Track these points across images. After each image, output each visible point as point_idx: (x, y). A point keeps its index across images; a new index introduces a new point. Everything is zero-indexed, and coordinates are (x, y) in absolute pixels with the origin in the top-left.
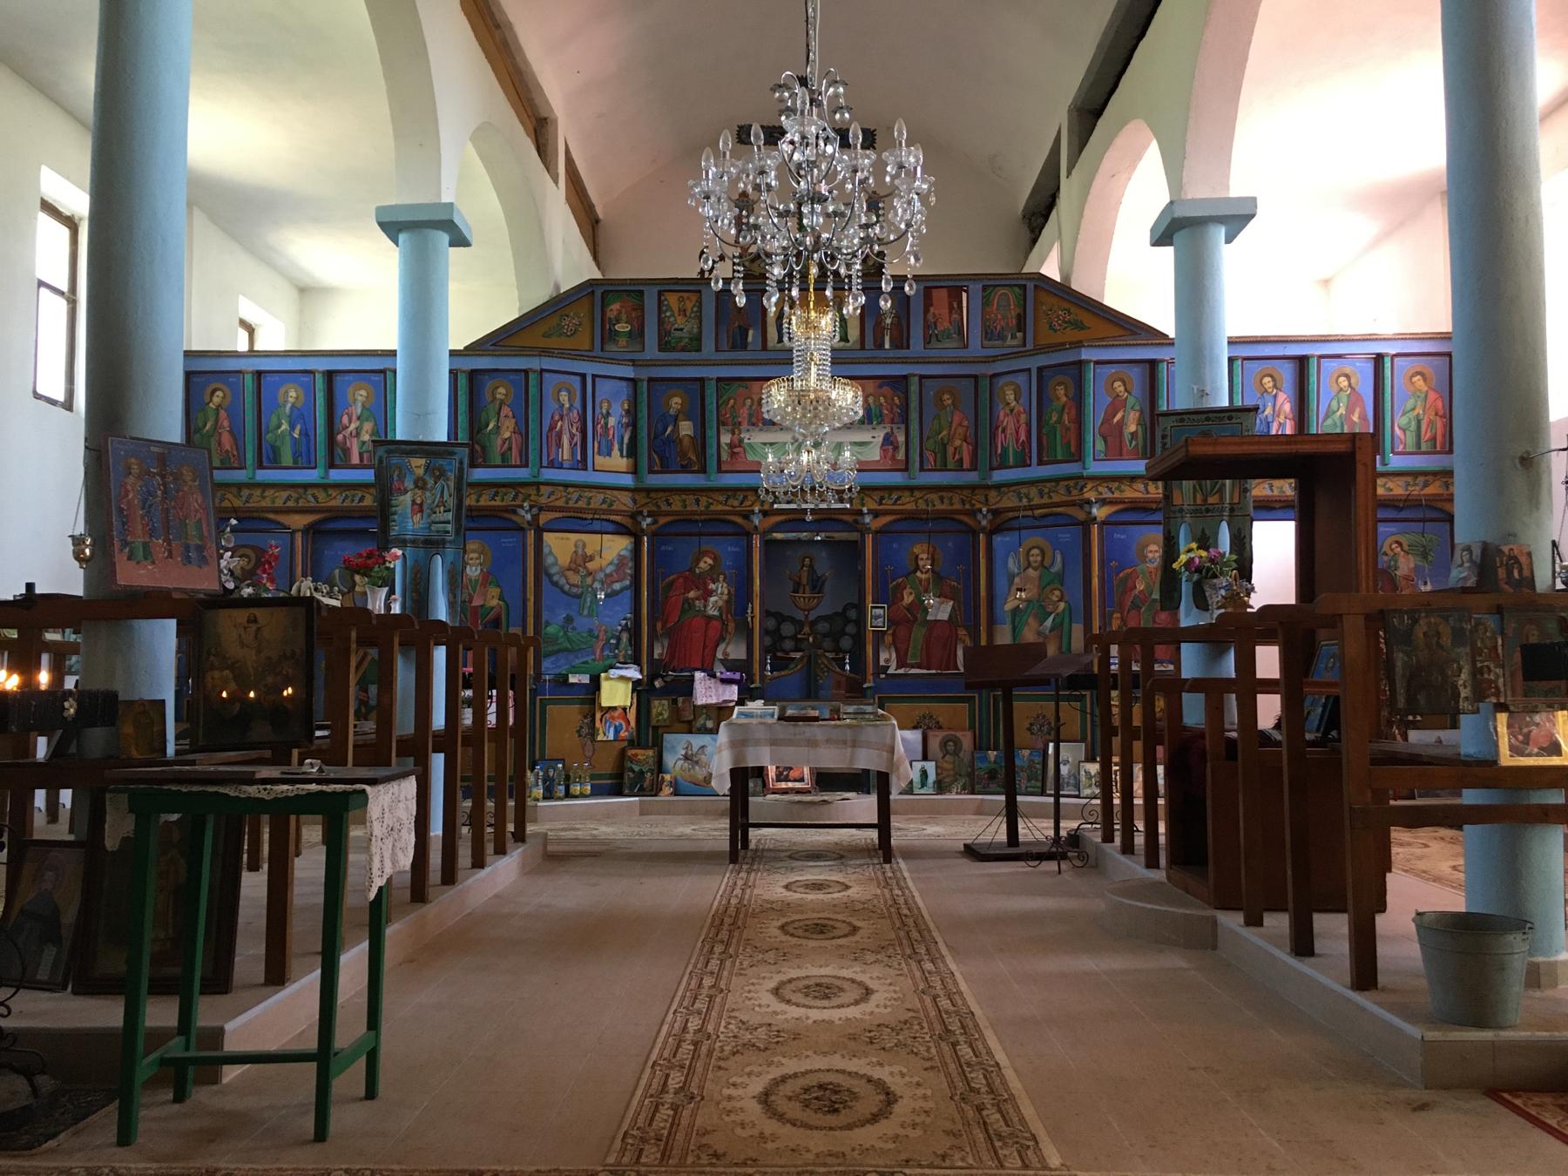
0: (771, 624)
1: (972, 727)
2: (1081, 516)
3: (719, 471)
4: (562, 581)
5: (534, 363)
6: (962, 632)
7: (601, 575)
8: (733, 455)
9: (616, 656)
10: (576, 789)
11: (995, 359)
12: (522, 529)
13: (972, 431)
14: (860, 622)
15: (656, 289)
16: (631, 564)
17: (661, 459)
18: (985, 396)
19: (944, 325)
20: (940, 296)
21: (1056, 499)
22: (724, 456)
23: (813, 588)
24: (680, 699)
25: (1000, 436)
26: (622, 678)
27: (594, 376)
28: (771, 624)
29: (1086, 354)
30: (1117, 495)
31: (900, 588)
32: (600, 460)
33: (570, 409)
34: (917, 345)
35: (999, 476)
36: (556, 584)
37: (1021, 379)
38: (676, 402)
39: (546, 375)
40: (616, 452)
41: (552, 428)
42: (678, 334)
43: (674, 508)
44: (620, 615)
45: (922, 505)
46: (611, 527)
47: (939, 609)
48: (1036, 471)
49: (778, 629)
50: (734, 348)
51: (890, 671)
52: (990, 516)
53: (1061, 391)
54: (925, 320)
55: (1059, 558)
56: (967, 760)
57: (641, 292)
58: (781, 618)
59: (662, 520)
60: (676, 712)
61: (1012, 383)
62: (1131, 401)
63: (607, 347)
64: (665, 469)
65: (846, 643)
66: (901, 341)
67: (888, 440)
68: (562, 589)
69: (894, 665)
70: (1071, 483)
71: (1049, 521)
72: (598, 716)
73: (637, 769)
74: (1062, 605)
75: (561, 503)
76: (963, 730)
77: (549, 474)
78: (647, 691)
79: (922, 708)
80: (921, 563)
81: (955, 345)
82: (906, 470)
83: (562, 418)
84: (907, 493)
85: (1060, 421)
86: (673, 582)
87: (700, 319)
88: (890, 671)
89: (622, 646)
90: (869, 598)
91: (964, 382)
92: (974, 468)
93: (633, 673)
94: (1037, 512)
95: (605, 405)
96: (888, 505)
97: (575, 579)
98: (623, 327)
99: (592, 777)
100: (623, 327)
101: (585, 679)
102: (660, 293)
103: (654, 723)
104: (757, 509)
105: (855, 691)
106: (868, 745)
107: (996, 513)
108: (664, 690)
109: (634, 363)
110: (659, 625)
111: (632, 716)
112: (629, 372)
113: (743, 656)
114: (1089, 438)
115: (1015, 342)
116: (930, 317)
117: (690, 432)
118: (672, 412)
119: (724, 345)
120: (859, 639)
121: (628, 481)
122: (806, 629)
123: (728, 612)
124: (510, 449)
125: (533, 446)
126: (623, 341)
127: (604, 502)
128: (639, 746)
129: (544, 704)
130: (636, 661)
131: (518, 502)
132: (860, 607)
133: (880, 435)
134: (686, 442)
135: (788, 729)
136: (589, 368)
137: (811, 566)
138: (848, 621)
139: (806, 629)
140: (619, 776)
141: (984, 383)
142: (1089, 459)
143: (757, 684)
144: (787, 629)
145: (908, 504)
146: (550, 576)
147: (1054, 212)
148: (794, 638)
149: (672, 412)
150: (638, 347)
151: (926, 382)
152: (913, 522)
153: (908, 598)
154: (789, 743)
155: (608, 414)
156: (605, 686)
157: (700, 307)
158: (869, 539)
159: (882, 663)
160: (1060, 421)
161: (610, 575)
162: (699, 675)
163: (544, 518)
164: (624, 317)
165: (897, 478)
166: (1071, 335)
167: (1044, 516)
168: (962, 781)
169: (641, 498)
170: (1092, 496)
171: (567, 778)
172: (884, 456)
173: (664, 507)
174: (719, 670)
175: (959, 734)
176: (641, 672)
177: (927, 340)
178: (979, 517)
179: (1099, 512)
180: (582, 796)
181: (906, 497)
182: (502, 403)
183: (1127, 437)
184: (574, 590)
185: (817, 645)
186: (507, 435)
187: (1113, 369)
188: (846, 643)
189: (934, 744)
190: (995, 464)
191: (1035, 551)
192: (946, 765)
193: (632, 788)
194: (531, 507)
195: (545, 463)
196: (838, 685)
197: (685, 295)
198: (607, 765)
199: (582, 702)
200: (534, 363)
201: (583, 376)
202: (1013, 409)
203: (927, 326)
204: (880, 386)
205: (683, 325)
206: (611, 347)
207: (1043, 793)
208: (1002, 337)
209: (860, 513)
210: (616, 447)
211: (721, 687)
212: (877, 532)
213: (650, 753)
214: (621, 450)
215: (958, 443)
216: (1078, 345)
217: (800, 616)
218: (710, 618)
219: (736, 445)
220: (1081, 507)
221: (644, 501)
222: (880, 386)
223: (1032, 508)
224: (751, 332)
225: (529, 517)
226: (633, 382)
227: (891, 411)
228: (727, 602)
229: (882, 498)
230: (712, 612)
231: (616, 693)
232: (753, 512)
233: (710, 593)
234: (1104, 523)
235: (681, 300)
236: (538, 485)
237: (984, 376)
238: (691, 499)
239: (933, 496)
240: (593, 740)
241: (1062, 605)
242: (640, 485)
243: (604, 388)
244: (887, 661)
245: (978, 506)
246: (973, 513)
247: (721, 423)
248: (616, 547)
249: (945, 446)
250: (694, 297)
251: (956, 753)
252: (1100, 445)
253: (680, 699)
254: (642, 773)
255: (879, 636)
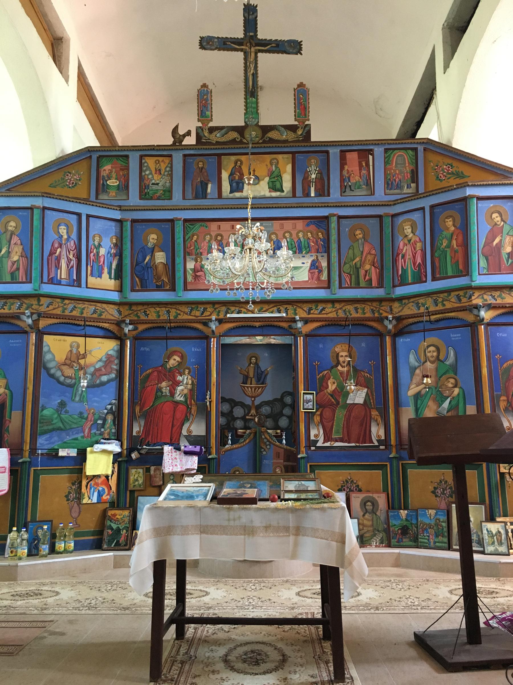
0: (226, 407)
1: (385, 490)
2: (470, 318)
3: (185, 289)
4: (59, 374)
5: (39, 202)
6: (374, 413)
7: (92, 369)
8: (196, 277)
9: (101, 434)
10: (60, 546)
11: (395, 203)
12: (26, 332)
13: (378, 258)
14: (294, 406)
15: (138, 154)
16: (116, 361)
17: (141, 281)
18: (387, 230)
19: (356, 179)
20: (352, 157)
21: (448, 305)
22: (190, 279)
23: (258, 381)
24: (152, 468)
25: (400, 261)
26: (104, 451)
27: (88, 216)
28: (226, 407)
29: (469, 191)
30: (499, 301)
31: (324, 380)
32: (92, 280)
33: (68, 240)
34: (335, 194)
35: (400, 291)
36: (52, 376)
37: (416, 216)
38: (153, 238)
39: (47, 212)
40: (105, 275)
41: (51, 253)
42: (155, 187)
43: (150, 317)
44: (106, 400)
45: (341, 314)
46: (101, 333)
47: (358, 396)
48: (430, 286)
49: (231, 412)
50: (196, 198)
51: (319, 444)
52: (394, 322)
53: (449, 223)
54: (341, 175)
55: (452, 353)
56: (383, 517)
57: (127, 157)
58: (233, 403)
59: (141, 327)
60: (149, 478)
61: (409, 220)
62: (506, 228)
63: (100, 197)
64: (144, 288)
65: (284, 422)
66: (323, 190)
67: (315, 266)
68: (59, 382)
69: (321, 439)
70: (461, 293)
71: (441, 324)
72: (84, 483)
73: (114, 526)
74: (456, 391)
75: (58, 312)
76: (377, 492)
77: (48, 289)
78: (126, 462)
79: (344, 474)
80: (341, 359)
81: (364, 193)
82: (329, 287)
83: (60, 246)
84: (330, 305)
85: (449, 246)
86: (149, 375)
87: (171, 176)
88: (319, 444)
89: (107, 426)
90: (301, 387)
91: (372, 221)
92: (380, 285)
93: (115, 447)
94: (433, 318)
95: (97, 239)
96: (315, 314)
97: (69, 372)
98: (113, 182)
99: (76, 535)
100: (113, 182)
101: (73, 453)
102: (141, 157)
103: (131, 487)
104: (214, 318)
105: (293, 468)
106: (314, 533)
107: (399, 319)
108: (140, 462)
109: (121, 208)
110: (137, 409)
111: (113, 482)
112: (117, 215)
113: (203, 433)
114: (474, 257)
115: (410, 191)
116: (345, 173)
117: (164, 261)
118: (150, 245)
119: (189, 194)
120: (294, 419)
121: (115, 296)
122: (253, 412)
123: (191, 399)
124: (18, 269)
125: (36, 265)
126: (113, 193)
127: (95, 312)
128: (119, 508)
129: (37, 474)
130: (119, 438)
131: (21, 311)
132: (294, 394)
133: (308, 261)
134: (160, 268)
135: (222, 514)
136: (84, 210)
137: (256, 364)
138: (285, 405)
139: (253, 412)
140: (100, 532)
141: (387, 221)
142: (475, 274)
143: (213, 456)
144: (238, 412)
145: (330, 312)
146: (47, 370)
147: (432, 109)
148: (243, 418)
149: (150, 245)
150: (125, 197)
151: (343, 221)
152: (335, 327)
153: (332, 387)
154: (222, 530)
155: (100, 245)
156: (90, 458)
157: (171, 167)
158: (301, 341)
159: (312, 438)
160: (449, 246)
161: (99, 369)
162: (167, 449)
163: (43, 323)
164: (114, 175)
165: (322, 294)
166: (453, 182)
167: (437, 321)
168: (378, 538)
169: (125, 310)
170: (478, 301)
171: (53, 536)
172: (311, 277)
173: (143, 317)
174: (184, 444)
175: (375, 496)
176: (122, 446)
177: (343, 189)
178: (386, 322)
179: (486, 315)
180: (66, 551)
181: (329, 308)
182: (12, 233)
183: (504, 256)
184: (68, 381)
185: (261, 424)
186: (16, 258)
187: (491, 204)
188: (284, 422)
189: (356, 502)
190: (397, 282)
191: (432, 348)
192: (365, 522)
193: (110, 543)
194: (32, 314)
195: (45, 280)
196: (278, 456)
197: (160, 159)
198: (90, 523)
199: (71, 471)
200: (39, 202)
201: (79, 215)
202: (411, 237)
203: (342, 180)
204: (308, 225)
205: (158, 181)
206: (103, 197)
207: (449, 548)
208: (399, 187)
209: (294, 321)
210: (106, 270)
211: (185, 458)
212: (307, 336)
213: (126, 513)
214: (110, 273)
215: (367, 267)
216: (465, 185)
217: (248, 401)
218: (177, 403)
219: (198, 271)
220: (471, 311)
221: (127, 313)
222: (308, 225)
223: (429, 314)
224: (210, 186)
225: (30, 321)
226: (120, 222)
227: (316, 243)
228: (191, 390)
229: (310, 309)
230: (179, 398)
231: (99, 462)
232: (211, 320)
233: (178, 383)
234: (488, 324)
235: (157, 162)
236: (38, 296)
237: (387, 215)
238: (163, 311)
239: (350, 308)
240: (79, 503)
241: (456, 391)
242: (124, 300)
243: (96, 226)
244: (316, 436)
245: (385, 314)
246: (380, 320)
247: (186, 253)
248: (101, 349)
249: (357, 269)
250: (167, 160)
251: (373, 512)
252: (483, 263)
253: (152, 468)
254: (118, 530)
255: (309, 415)
